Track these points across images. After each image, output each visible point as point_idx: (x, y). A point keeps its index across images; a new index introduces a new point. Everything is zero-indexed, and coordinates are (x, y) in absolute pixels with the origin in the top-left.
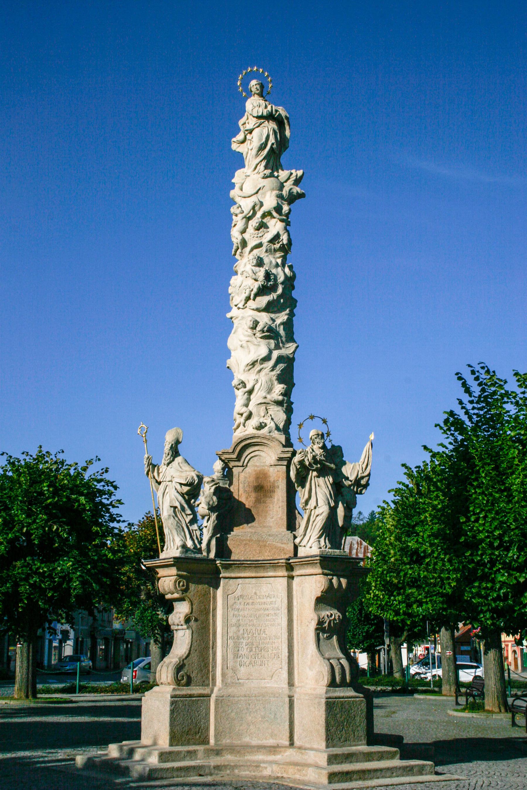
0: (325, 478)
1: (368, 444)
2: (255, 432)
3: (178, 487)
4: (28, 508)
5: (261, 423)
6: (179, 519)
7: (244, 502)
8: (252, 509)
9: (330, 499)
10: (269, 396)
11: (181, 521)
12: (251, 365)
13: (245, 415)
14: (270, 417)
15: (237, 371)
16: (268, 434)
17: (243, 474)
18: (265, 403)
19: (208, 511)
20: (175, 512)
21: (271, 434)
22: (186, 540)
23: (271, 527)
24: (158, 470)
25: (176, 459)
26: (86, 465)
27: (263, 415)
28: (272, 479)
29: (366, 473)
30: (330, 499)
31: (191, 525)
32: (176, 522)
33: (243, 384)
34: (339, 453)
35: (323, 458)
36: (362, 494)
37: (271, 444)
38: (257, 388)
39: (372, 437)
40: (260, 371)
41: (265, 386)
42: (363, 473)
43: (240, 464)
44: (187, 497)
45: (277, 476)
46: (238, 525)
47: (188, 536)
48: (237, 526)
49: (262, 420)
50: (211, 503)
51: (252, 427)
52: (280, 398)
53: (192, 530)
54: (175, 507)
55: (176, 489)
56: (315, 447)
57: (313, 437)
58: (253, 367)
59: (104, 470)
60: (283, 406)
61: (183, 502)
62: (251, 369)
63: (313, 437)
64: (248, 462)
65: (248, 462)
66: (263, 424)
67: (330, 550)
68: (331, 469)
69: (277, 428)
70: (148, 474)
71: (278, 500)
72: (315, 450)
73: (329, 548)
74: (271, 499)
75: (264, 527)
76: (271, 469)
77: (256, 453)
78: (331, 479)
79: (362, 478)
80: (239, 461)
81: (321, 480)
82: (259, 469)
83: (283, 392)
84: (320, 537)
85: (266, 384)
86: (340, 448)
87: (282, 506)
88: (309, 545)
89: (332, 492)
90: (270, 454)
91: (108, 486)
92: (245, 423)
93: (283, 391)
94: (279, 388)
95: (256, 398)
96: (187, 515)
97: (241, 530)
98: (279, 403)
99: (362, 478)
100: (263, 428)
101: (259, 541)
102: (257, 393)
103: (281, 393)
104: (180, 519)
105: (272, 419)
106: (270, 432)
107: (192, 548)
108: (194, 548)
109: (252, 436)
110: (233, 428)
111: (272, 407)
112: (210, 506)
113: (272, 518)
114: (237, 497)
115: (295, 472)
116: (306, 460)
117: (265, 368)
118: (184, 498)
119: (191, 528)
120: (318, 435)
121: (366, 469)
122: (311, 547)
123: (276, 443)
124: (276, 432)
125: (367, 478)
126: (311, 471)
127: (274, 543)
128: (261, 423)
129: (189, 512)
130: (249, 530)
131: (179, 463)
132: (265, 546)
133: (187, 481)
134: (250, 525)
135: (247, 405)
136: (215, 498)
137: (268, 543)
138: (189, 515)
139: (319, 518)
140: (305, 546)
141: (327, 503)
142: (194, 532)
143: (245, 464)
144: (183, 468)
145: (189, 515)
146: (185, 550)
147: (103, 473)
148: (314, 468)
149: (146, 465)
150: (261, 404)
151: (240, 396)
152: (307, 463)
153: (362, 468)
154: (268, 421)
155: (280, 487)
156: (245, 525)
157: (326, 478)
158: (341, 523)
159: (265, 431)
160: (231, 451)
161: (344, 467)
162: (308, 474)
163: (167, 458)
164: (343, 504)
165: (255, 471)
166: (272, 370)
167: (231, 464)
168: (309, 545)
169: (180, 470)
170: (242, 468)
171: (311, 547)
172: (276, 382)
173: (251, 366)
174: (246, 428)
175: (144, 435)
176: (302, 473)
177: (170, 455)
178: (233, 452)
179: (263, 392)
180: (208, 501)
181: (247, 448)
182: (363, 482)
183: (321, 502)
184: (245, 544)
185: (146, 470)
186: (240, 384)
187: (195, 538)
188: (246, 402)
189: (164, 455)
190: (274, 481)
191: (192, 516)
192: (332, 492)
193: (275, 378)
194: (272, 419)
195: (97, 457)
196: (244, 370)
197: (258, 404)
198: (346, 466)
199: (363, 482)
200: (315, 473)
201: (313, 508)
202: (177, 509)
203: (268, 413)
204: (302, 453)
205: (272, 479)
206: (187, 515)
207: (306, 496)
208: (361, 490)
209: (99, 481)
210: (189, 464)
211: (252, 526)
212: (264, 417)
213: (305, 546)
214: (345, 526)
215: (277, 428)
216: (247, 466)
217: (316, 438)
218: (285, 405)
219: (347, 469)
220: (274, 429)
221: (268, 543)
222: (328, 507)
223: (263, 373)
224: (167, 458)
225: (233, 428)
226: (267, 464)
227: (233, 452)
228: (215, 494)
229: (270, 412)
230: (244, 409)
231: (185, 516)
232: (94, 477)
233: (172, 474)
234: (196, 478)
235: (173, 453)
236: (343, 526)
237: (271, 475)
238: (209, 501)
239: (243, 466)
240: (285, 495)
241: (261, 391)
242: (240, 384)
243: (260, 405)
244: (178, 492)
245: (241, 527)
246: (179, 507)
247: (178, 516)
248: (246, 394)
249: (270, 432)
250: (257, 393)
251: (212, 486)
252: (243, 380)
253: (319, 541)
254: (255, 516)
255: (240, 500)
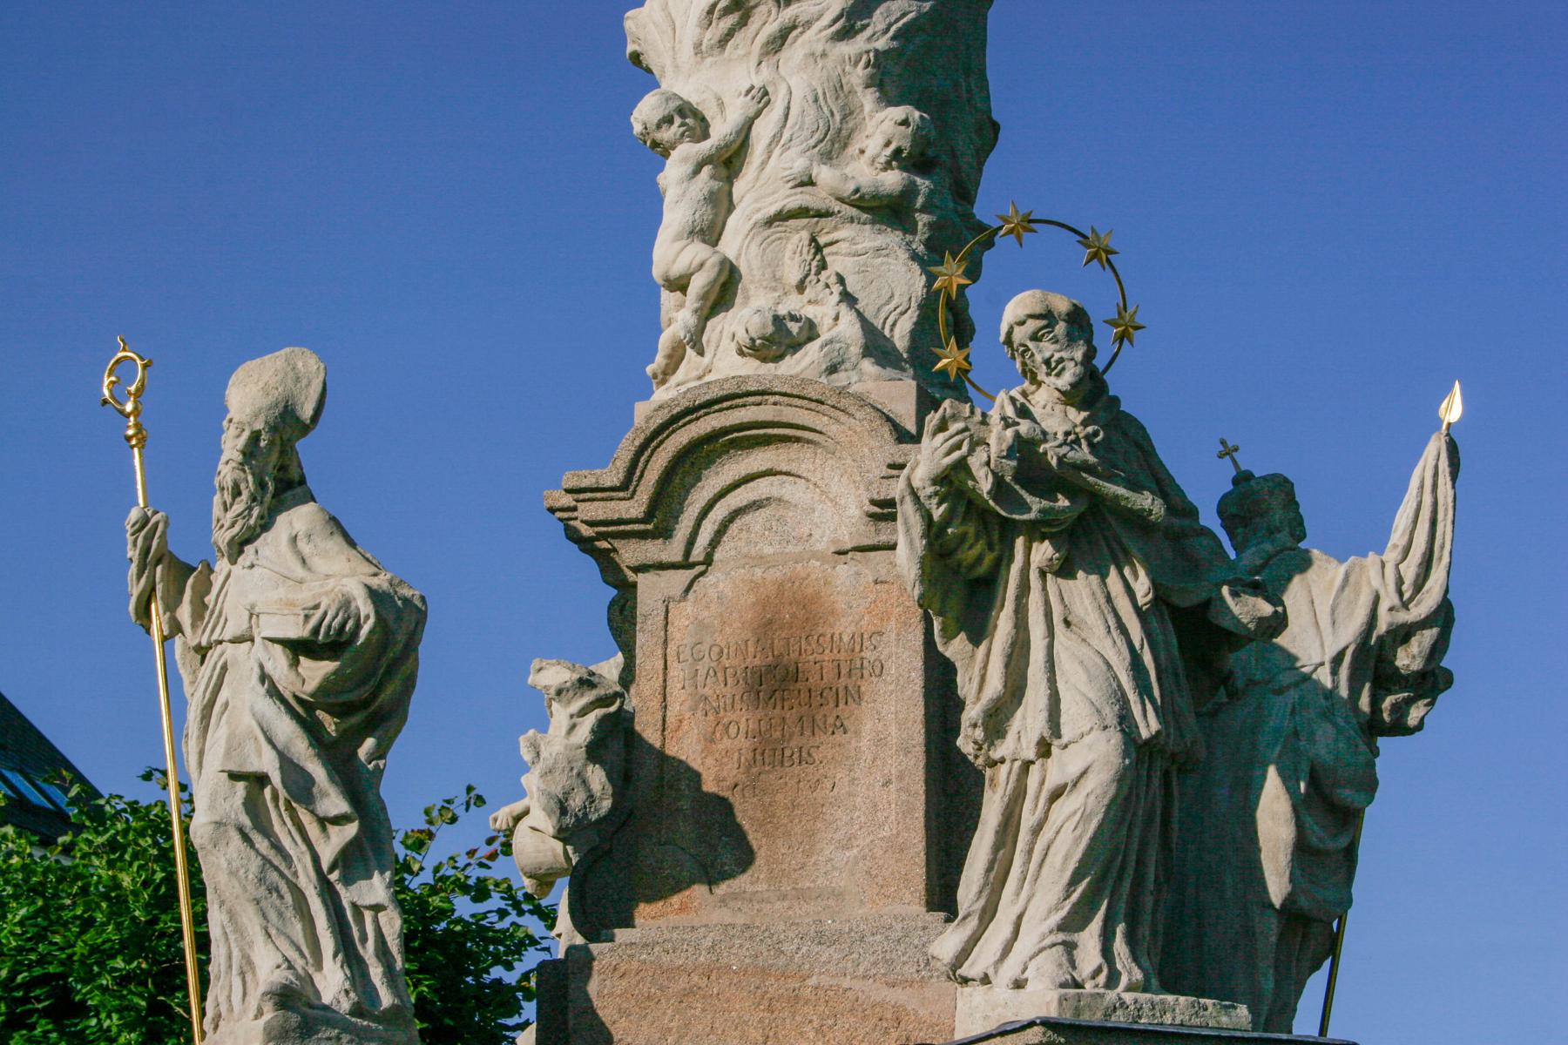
0: (1104, 577)
1: (1435, 448)
2: (752, 369)
3: (278, 664)
4: (152, 1001)
5: (778, 320)
6: (277, 847)
7: (695, 765)
8: (736, 800)
9: (1133, 697)
10: (825, 175)
11: (286, 857)
12: (727, 11)
13: (697, 284)
14: (837, 289)
15: (669, 70)
16: (823, 380)
17: (688, 607)
18: (802, 212)
19: (559, 845)
20: (253, 805)
21: (840, 379)
22: (319, 965)
23: (839, 895)
24: (204, 587)
25: (282, 520)
26: (425, 827)
27: (793, 276)
28: (845, 628)
29: (1419, 611)
30: (1133, 697)
31: (348, 880)
32: (255, 864)
33: (692, 119)
34: (1277, 516)
35: (1084, 454)
36: (1410, 731)
37: (833, 429)
38: (763, 131)
39: (1453, 409)
40: (780, 39)
41: (804, 117)
42: (1406, 606)
43: (672, 550)
44: (330, 724)
45: (877, 604)
46: (659, 891)
47: (327, 943)
48: (650, 900)
49: (792, 304)
50: (577, 801)
51: (734, 346)
52: (893, 180)
53: (354, 905)
54: (261, 780)
55: (264, 677)
56: (1044, 400)
57: (1020, 335)
58: (743, 22)
59: (496, 845)
60: (908, 227)
61: (301, 749)
62: (730, 34)
63: (1020, 335)
64: (715, 543)
65: (715, 543)
66: (794, 327)
67: (1128, 997)
68: (1138, 522)
69: (876, 346)
70: (144, 612)
71: (880, 742)
72: (1036, 411)
73: (1130, 988)
74: (839, 737)
75: (802, 896)
76: (844, 572)
77: (761, 488)
78: (1142, 586)
79: (1403, 634)
80: (665, 533)
81: (1081, 590)
82: (775, 574)
83: (906, 144)
84: (1074, 922)
85: (812, 112)
86: (1282, 486)
87: (900, 777)
88: (1010, 969)
89: (1147, 658)
90: (835, 489)
91: (521, 913)
92: (701, 329)
93: (903, 138)
94: (883, 126)
95: (761, 189)
96: (324, 822)
97: (673, 919)
98: (888, 211)
99: (1403, 634)
100: (795, 346)
101: (765, 972)
102: (764, 164)
103: (898, 152)
104: (286, 843)
105: (848, 298)
106: (833, 369)
107: (345, 1006)
108: (357, 1011)
109: (730, 388)
110: (650, 369)
111: (845, 232)
112: (569, 820)
113: (846, 848)
114: (652, 736)
115: (920, 544)
116: (975, 462)
117: (808, 24)
118: (311, 729)
119: (346, 896)
120: (1048, 316)
121: (1419, 586)
122: (1019, 984)
123: (861, 421)
124: (868, 366)
125: (1429, 636)
126: (1020, 542)
127: (846, 983)
128: (778, 320)
129: (334, 802)
130: (723, 916)
131: (294, 539)
132: (795, 999)
133: (313, 622)
134: (722, 889)
135: (710, 233)
136: (597, 777)
137: (813, 981)
138: (339, 820)
139: (1068, 806)
140: (985, 980)
141: (1111, 719)
142: (368, 916)
143: (698, 553)
144: (317, 563)
145: (339, 820)
146: (294, 1019)
147: (493, 856)
148: (1032, 516)
149: (133, 568)
150: (782, 217)
151: (680, 187)
152: (985, 485)
153: (1400, 581)
154: (822, 308)
155: (891, 669)
156: (699, 890)
157: (1113, 578)
158: (1277, 888)
159: (804, 363)
160: (612, 477)
161: (1297, 579)
162: (1006, 558)
163: (231, 515)
164: (1288, 779)
165: (754, 587)
166: (846, 34)
167: (629, 553)
168: (1010, 969)
169: (300, 572)
170: (686, 575)
171: (1019, 984)
172: (868, 99)
173: (731, 20)
174: (706, 360)
175: (129, 407)
176: (968, 555)
177: (245, 495)
178: (627, 485)
179: (793, 152)
180: (558, 791)
181: (709, 461)
182: (1409, 658)
183: (1075, 716)
184: (689, 993)
185: (136, 590)
186: (669, 120)
187: (368, 952)
188: (707, 214)
189: (217, 499)
190: (859, 639)
191: (352, 829)
192: (1147, 658)
193: (859, 75)
194: (848, 298)
195: (470, 789)
196: (698, 46)
197: (769, 222)
198: (1311, 574)
199: (1409, 658)
200: (1043, 552)
201: (1030, 754)
202: (267, 791)
203: (823, 266)
204: (955, 427)
205: (845, 628)
206: (324, 822)
207: (995, 684)
208: (1400, 710)
209: (480, 892)
210: (352, 544)
211: (735, 896)
212: (801, 287)
213: (985, 980)
214: (1303, 902)
215: (876, 346)
216: (708, 561)
217: (1035, 337)
218: (922, 219)
219: (1315, 592)
220: (855, 350)
221: (813, 981)
222: (1115, 738)
223: (795, 52)
224: (231, 515)
225: (650, 369)
226: (820, 546)
227: (624, 486)
228: (594, 751)
229: (838, 262)
230: (697, 251)
231: (313, 830)
232: (451, 872)
233: (252, 598)
234: (365, 607)
235: (261, 485)
236: (1290, 900)
237: (841, 606)
238: (567, 794)
239: (685, 565)
240: (919, 712)
241: (786, 148)
242: (669, 120)
243: (778, 228)
244: (274, 692)
245: (676, 900)
246: (276, 778)
247: (277, 827)
248: (707, 170)
249: (833, 369)
250: (764, 164)
251: (583, 712)
252: (694, 99)
253: (1070, 947)
254: (754, 838)
255: (671, 750)
